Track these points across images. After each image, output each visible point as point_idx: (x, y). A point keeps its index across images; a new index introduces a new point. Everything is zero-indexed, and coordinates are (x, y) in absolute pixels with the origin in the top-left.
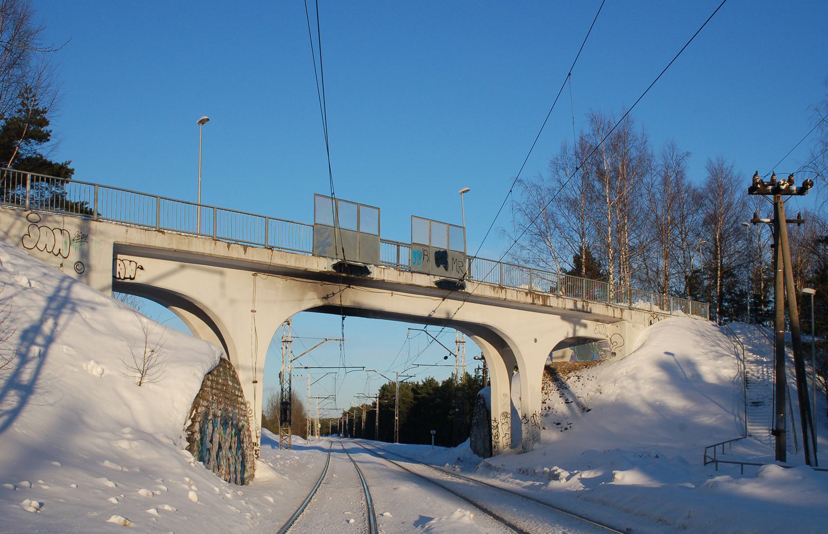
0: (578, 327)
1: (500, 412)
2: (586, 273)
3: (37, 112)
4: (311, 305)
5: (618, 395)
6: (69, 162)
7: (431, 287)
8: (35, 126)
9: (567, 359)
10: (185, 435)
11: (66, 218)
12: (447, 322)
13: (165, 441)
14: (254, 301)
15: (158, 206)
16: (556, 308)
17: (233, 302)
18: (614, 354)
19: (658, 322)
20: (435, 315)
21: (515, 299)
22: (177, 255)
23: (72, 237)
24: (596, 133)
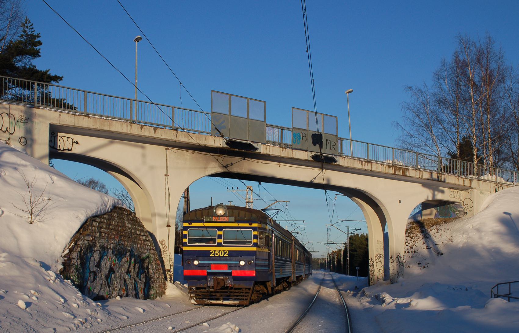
0: (436, 193)
1: (375, 254)
2: (464, 157)
3: (33, 37)
4: (213, 171)
5: (465, 243)
6: (49, 70)
7: (308, 160)
8: (30, 45)
9: (432, 217)
10: (61, 260)
11: (11, 105)
12: (327, 187)
13: (33, 263)
14: (167, 167)
15: (86, 98)
16: (414, 178)
17: (152, 168)
18: (466, 213)
19: (502, 190)
20: (316, 181)
21: (379, 170)
22: (382, 175)
23: (17, 119)
24: (463, 50)
